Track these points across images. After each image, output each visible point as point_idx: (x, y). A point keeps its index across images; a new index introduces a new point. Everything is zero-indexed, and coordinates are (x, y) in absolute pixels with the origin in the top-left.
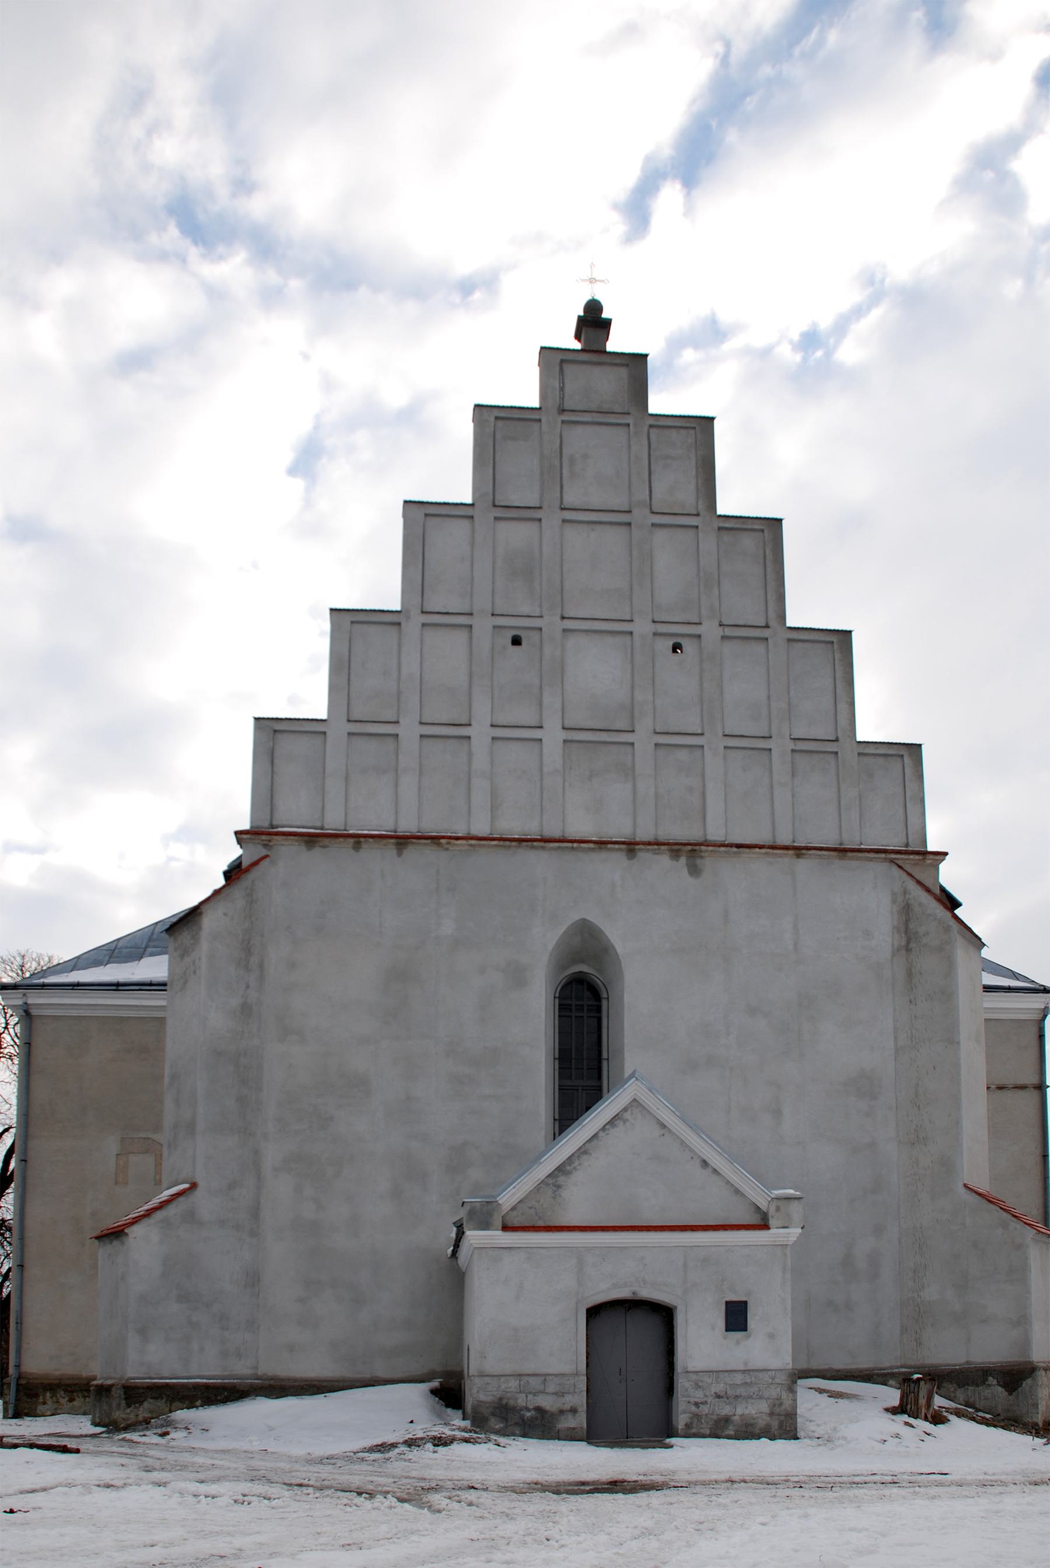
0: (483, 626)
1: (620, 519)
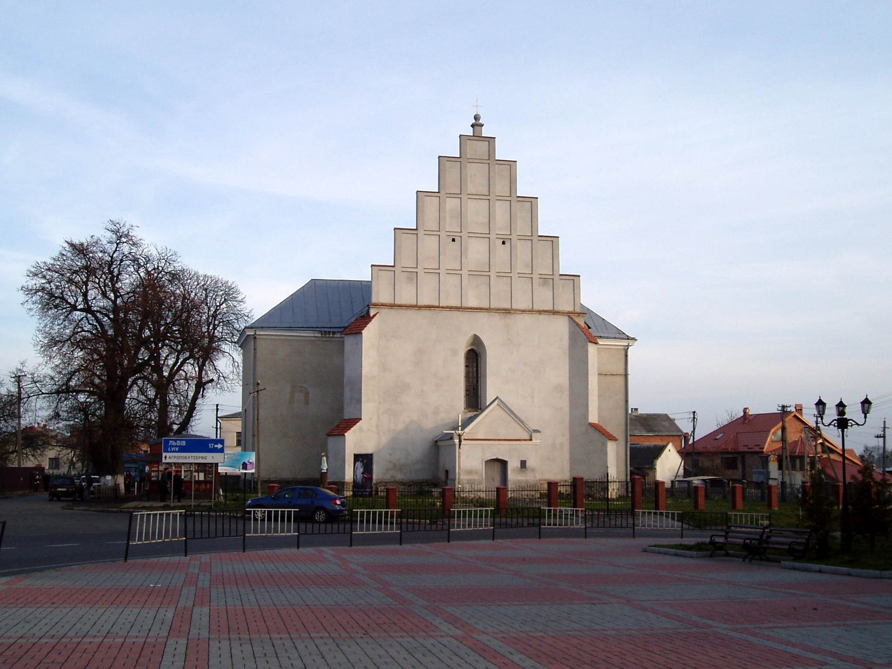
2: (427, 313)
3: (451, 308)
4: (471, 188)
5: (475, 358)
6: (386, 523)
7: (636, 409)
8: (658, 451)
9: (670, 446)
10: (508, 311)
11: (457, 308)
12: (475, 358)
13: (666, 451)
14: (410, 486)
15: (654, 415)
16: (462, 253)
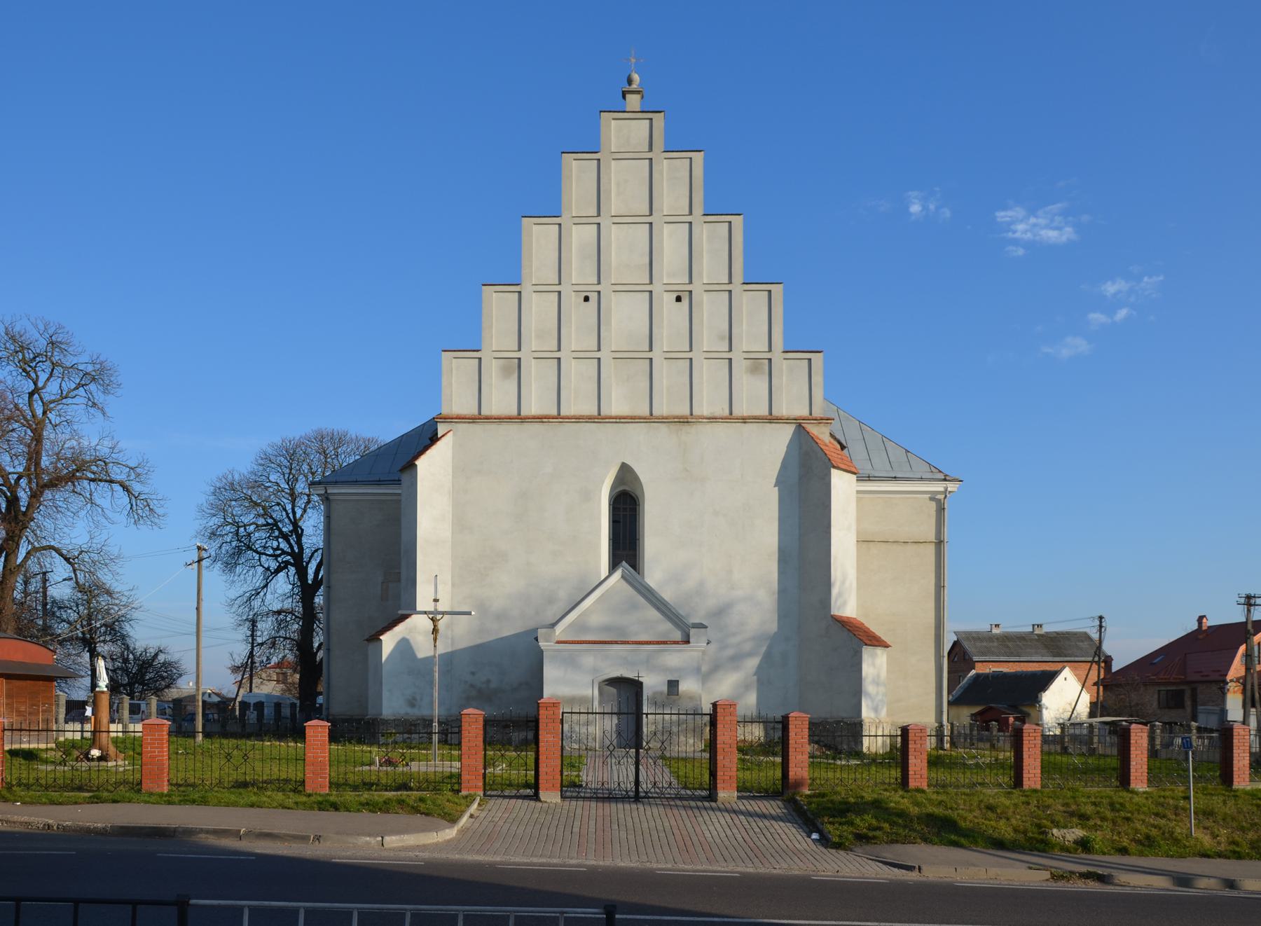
4: (615, 204)
5: (626, 510)
7: (1040, 626)
8: (1047, 679)
9: (1067, 672)
10: (683, 421)
11: (589, 419)
12: (626, 510)
13: (1058, 683)
15: (1068, 633)
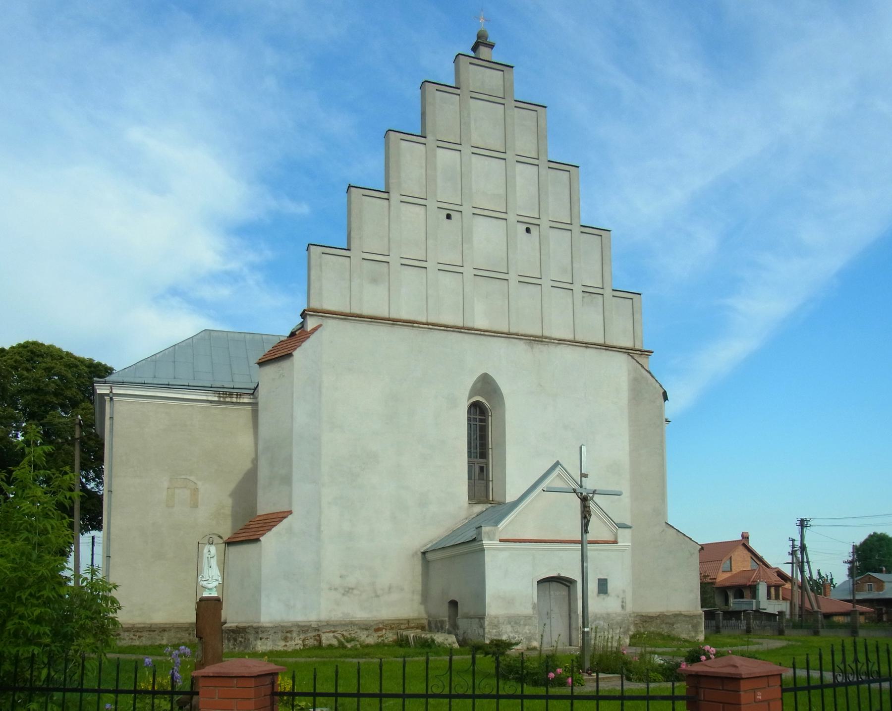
0: (432, 205)
1: (499, 155)
2: (406, 331)
3: (447, 328)
6: (871, 648)
14: (378, 630)
16: (466, 237)
